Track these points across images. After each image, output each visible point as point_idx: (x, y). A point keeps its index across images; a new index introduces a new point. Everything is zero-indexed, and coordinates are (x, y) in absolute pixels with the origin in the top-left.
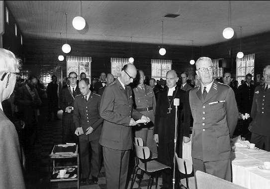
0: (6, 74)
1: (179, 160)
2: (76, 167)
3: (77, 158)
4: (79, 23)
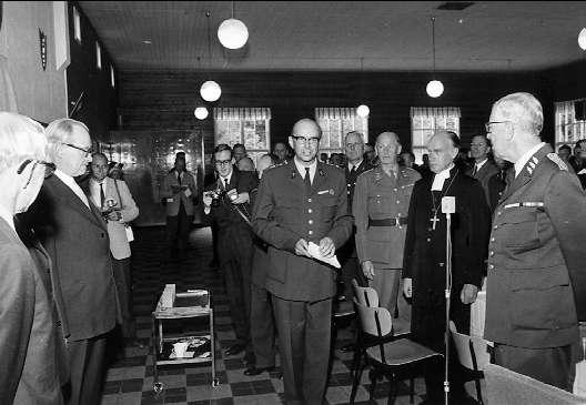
0: (28, 162)
1: (463, 339)
2: (208, 337)
3: (209, 316)
4: (233, 35)
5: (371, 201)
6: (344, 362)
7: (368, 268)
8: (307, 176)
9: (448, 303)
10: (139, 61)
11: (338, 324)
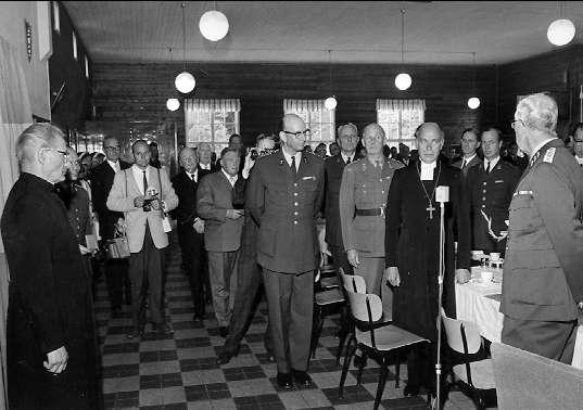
1: (449, 321)
5: (358, 191)
6: (329, 349)
7: (353, 257)
8: (294, 163)
9: (441, 288)
10: (112, 52)
11: (320, 312)
